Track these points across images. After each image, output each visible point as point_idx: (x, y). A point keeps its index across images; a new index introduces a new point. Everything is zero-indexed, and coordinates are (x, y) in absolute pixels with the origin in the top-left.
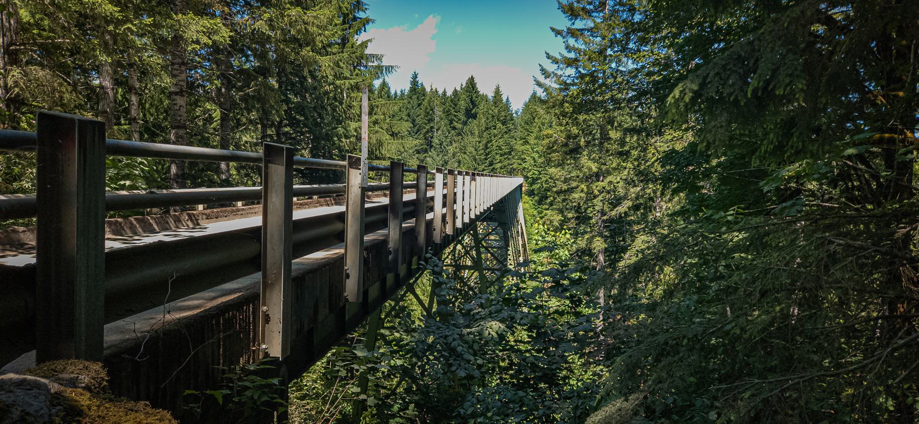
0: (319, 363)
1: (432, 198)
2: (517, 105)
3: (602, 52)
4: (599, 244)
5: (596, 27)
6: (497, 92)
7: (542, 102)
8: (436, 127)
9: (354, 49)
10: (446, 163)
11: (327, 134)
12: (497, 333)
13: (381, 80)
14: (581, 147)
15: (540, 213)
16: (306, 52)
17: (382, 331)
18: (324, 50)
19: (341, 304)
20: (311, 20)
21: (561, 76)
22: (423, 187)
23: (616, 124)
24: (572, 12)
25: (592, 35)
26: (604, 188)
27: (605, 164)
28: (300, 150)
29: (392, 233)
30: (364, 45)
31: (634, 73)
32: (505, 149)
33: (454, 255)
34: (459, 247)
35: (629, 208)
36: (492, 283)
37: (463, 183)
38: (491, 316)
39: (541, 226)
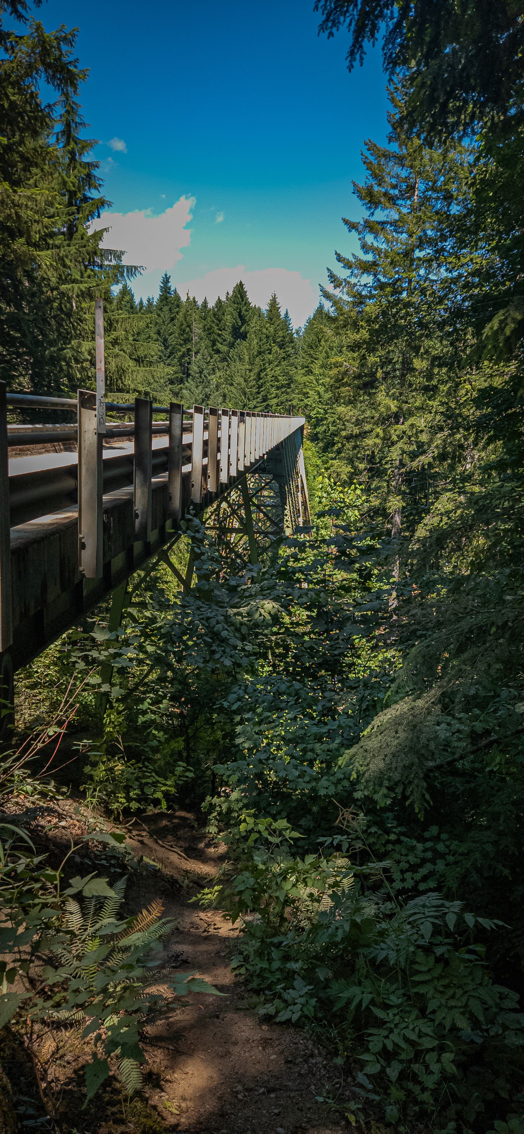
0: (52, 646)
1: (190, 446)
2: (298, 323)
3: (407, 254)
4: (395, 503)
5: (402, 220)
6: (274, 304)
7: (330, 319)
8: (194, 349)
9: (84, 242)
10: (207, 397)
11: (52, 357)
12: (270, 613)
13: (120, 286)
14: (377, 380)
15: (325, 462)
16: (19, 244)
17: (129, 610)
18: (45, 242)
19: (76, 581)
20: (23, 201)
21: (355, 285)
22: (177, 431)
23: (422, 350)
24: (371, 200)
25: (395, 231)
26: (404, 432)
27: (406, 402)
28: (17, 377)
29: (137, 493)
30: (98, 236)
31: (448, 284)
32: (283, 380)
33: (218, 515)
34: (224, 505)
35: (434, 458)
36: (265, 550)
37: (228, 427)
38: (264, 593)
39: (327, 480)
